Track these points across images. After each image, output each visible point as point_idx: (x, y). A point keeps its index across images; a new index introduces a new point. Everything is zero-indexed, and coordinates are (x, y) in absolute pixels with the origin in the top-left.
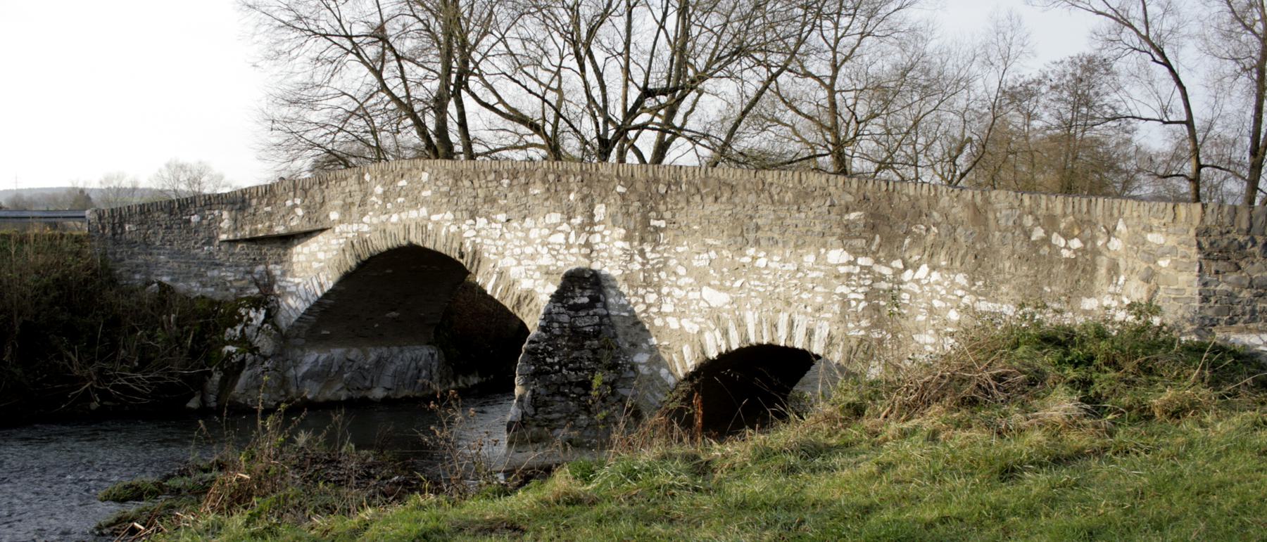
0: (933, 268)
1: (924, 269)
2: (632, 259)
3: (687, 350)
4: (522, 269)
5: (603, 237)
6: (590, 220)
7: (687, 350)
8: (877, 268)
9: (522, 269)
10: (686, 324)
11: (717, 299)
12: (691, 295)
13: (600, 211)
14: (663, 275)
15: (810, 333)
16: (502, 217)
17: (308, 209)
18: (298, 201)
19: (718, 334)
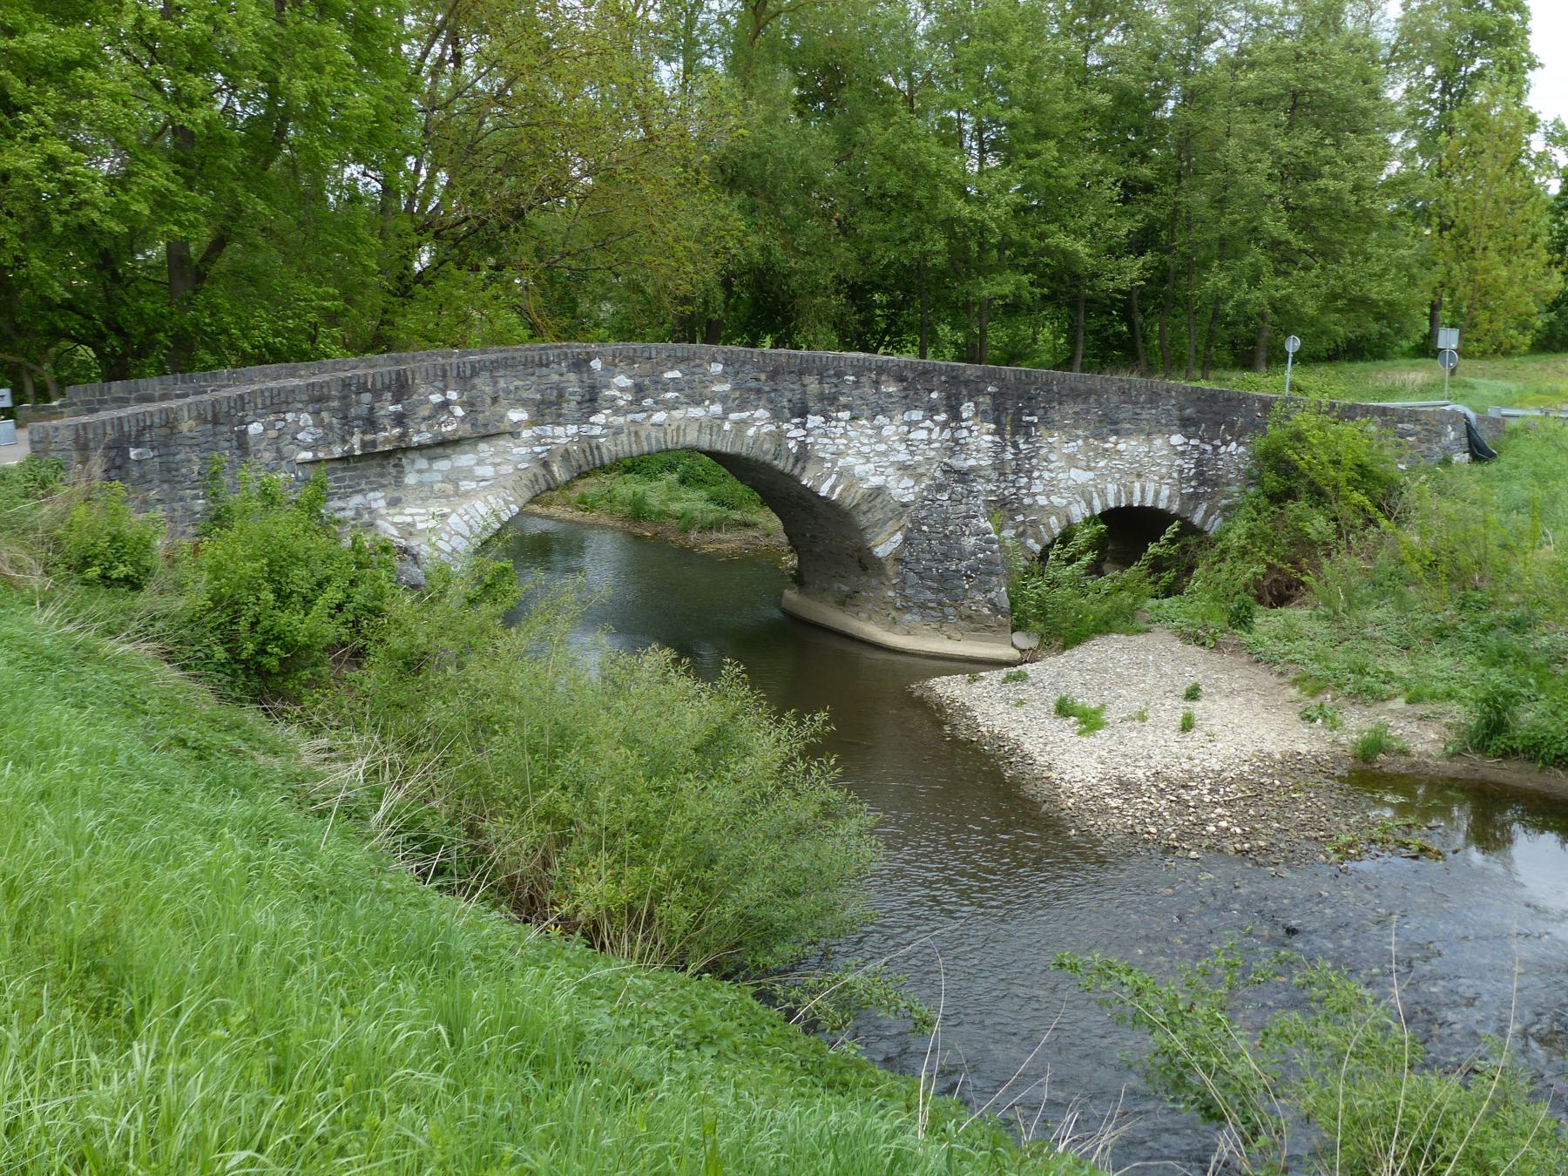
0: (1239, 444)
1: (1234, 444)
2: (1004, 451)
3: (1053, 520)
4: (871, 466)
5: (971, 431)
6: (955, 415)
7: (1053, 520)
8: (1203, 446)
9: (871, 466)
10: (1055, 499)
11: (1080, 476)
12: (1061, 476)
13: (967, 409)
14: (1034, 461)
15: (1157, 494)
16: (846, 415)
17: (471, 406)
18: (453, 395)
19: (1083, 504)
